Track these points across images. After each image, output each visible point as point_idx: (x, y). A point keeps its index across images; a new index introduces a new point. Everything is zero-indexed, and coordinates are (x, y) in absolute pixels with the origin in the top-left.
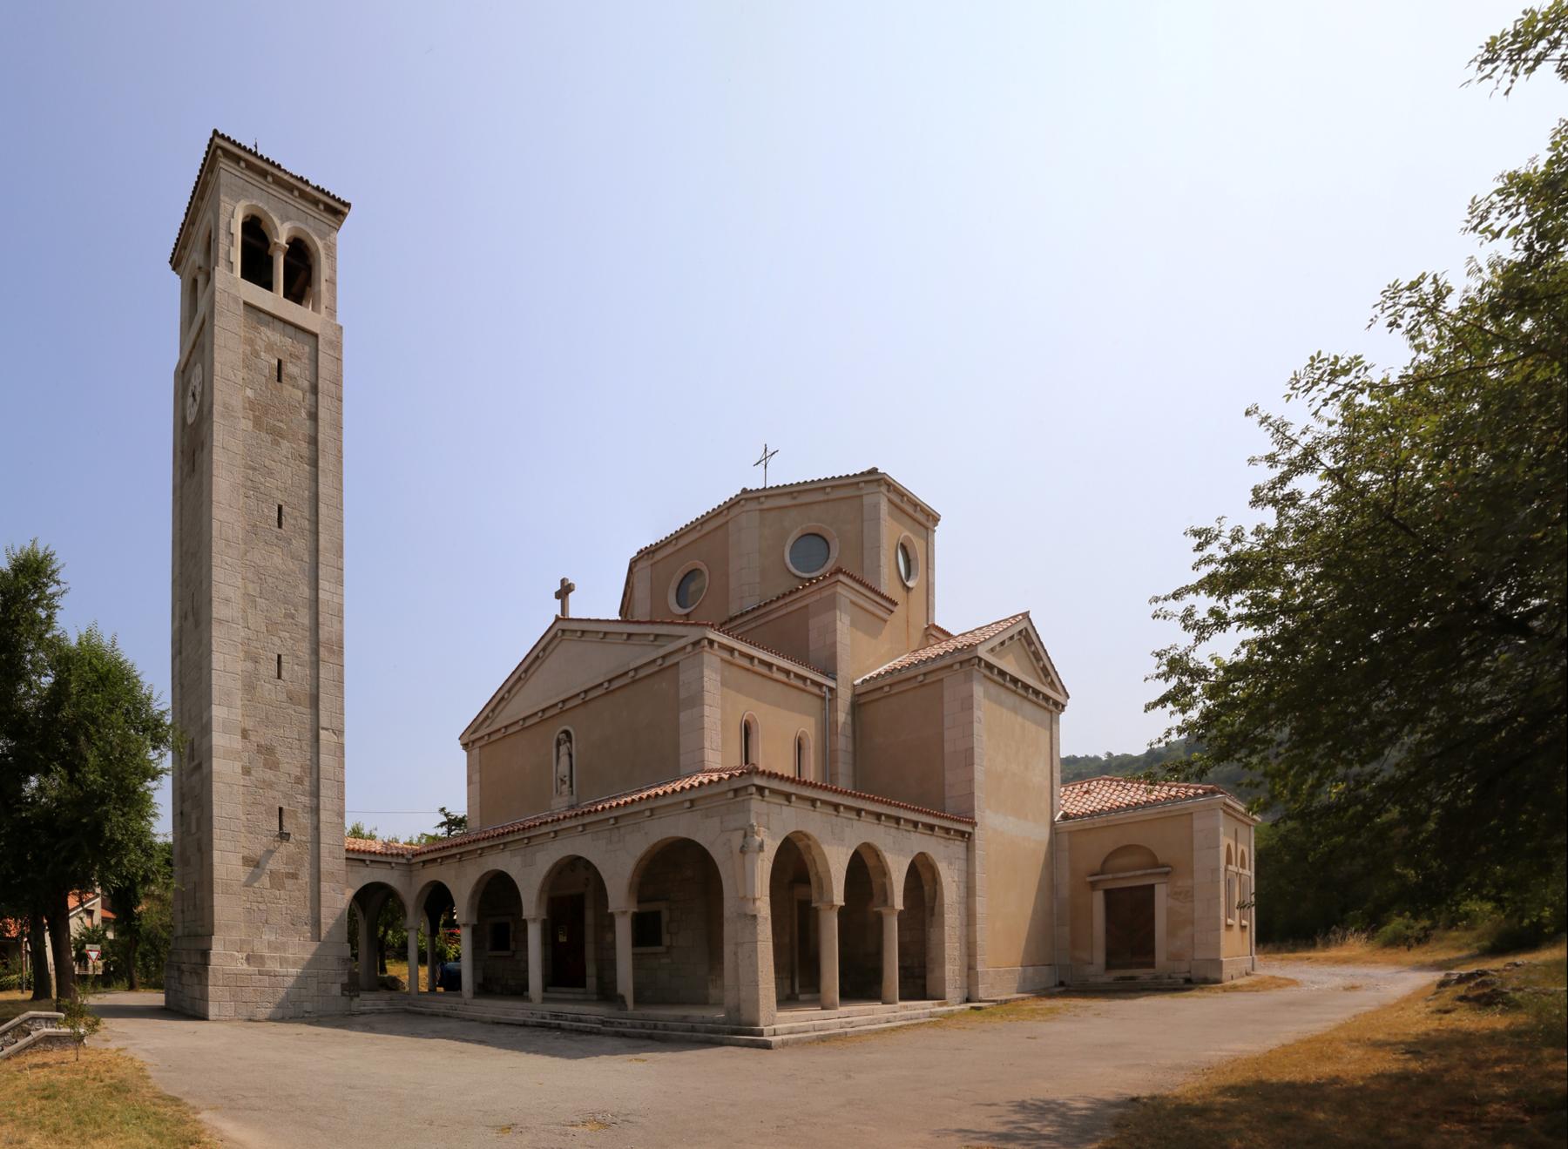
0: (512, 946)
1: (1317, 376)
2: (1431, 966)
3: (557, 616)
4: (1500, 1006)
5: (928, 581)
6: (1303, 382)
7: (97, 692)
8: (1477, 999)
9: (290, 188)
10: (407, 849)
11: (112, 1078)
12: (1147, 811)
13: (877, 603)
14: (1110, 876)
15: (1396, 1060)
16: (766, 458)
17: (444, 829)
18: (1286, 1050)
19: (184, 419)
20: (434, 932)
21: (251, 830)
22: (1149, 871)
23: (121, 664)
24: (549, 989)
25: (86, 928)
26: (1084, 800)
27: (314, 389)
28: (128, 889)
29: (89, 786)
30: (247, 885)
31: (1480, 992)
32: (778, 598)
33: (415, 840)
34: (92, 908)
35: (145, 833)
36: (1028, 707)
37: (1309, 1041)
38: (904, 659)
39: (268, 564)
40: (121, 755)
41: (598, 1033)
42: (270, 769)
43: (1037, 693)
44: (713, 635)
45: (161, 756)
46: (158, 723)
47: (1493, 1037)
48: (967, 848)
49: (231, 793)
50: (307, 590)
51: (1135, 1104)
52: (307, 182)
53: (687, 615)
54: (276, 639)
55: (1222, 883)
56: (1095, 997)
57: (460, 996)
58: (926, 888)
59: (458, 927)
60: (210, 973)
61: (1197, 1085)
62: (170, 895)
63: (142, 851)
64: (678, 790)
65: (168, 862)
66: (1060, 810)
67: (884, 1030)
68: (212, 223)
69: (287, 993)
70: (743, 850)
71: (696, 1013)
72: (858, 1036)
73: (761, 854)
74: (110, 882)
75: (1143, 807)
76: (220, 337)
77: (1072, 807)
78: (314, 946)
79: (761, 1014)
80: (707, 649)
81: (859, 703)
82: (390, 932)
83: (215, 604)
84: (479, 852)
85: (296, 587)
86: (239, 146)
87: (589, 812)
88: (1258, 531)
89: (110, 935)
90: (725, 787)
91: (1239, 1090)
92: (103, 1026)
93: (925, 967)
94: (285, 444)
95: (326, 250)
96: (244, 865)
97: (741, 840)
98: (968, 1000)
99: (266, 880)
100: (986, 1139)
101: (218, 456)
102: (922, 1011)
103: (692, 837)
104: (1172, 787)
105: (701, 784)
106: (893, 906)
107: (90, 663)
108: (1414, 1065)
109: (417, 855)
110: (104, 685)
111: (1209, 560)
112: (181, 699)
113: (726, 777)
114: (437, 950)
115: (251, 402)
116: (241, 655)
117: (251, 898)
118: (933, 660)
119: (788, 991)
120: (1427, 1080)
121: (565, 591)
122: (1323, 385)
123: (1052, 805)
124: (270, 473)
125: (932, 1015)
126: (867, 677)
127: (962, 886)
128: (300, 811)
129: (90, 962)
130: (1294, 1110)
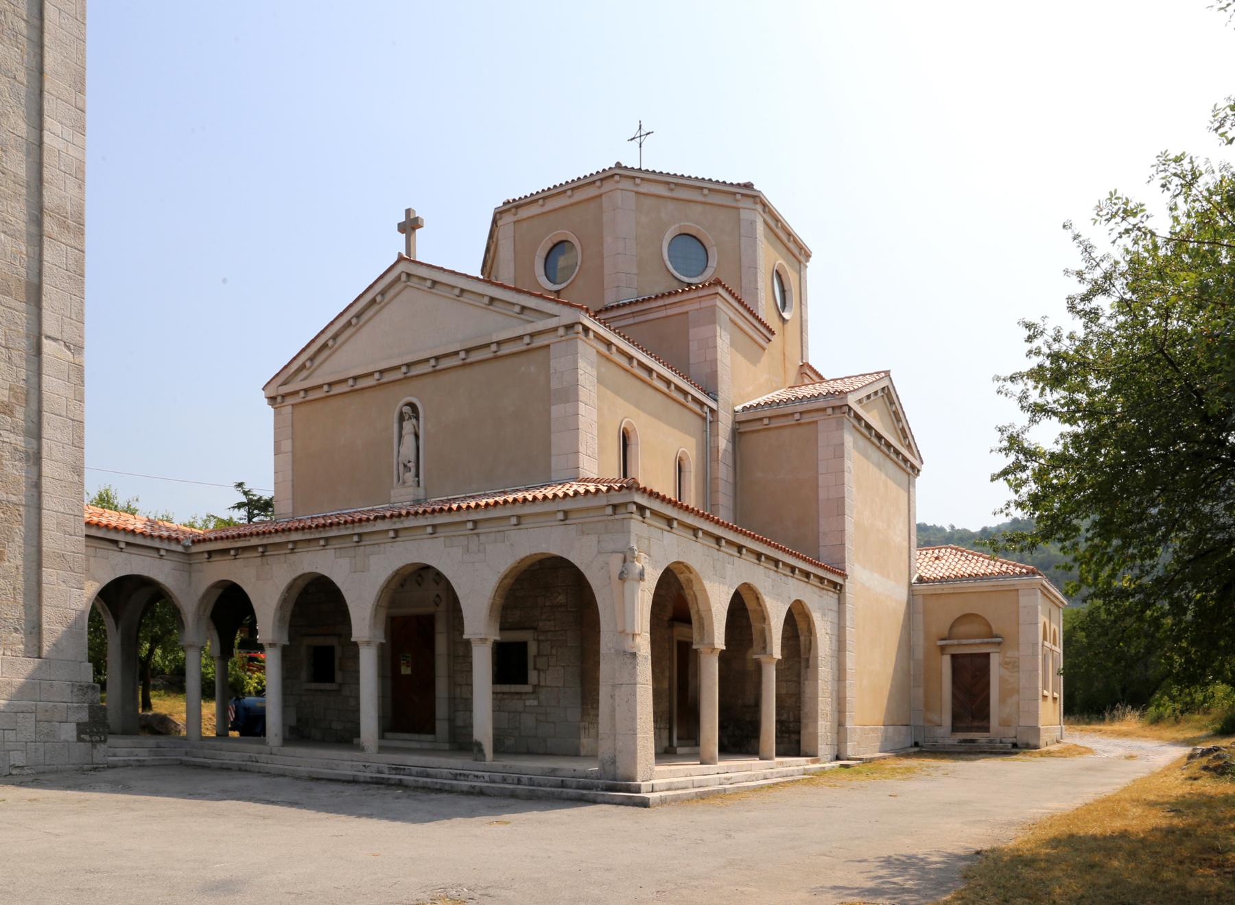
0: (339, 676)
1: (1114, 210)
2: (1182, 742)
3: (399, 253)
4: (1230, 775)
5: (801, 317)
6: (1104, 212)
8: (1215, 769)
10: (184, 532)
12: (985, 583)
13: (755, 327)
14: (955, 642)
15: (1165, 817)
16: (640, 136)
17: (243, 512)
18: (1089, 809)
20: (226, 652)
22: (986, 640)
24: (389, 735)
26: (935, 566)
31: (1217, 763)
32: (657, 297)
33: (199, 523)
36: (890, 465)
37: (1104, 801)
38: (781, 394)
41: (451, 791)
43: (897, 453)
44: (589, 322)
47: (1227, 801)
48: (839, 599)
51: (979, 857)
53: (558, 292)
55: (1040, 657)
56: (943, 758)
57: (264, 743)
58: (802, 638)
61: (1026, 839)
64: (550, 497)
66: (916, 572)
67: (762, 787)
70: (622, 577)
71: (566, 766)
72: (737, 793)
73: (641, 583)
75: (982, 579)
77: (926, 571)
78: (31, 665)
79: (639, 768)
80: (582, 336)
81: (738, 433)
82: (158, 651)
84: (290, 546)
87: (441, 510)
88: (1071, 337)
90: (602, 501)
91: (1056, 842)
93: (800, 722)
97: (621, 564)
98: (838, 758)
100: (857, 895)
102: (796, 768)
103: (565, 556)
104: (1003, 563)
105: (576, 493)
106: (772, 655)
108: (1176, 821)
109: (199, 541)
111: (1038, 353)
113: (604, 489)
118: (809, 399)
119: (666, 743)
120: (1187, 833)
121: (410, 225)
122: (1118, 219)
123: (910, 566)
125: (805, 772)
126: (747, 404)
127: (834, 638)
128: (7, 455)
130: (1097, 859)
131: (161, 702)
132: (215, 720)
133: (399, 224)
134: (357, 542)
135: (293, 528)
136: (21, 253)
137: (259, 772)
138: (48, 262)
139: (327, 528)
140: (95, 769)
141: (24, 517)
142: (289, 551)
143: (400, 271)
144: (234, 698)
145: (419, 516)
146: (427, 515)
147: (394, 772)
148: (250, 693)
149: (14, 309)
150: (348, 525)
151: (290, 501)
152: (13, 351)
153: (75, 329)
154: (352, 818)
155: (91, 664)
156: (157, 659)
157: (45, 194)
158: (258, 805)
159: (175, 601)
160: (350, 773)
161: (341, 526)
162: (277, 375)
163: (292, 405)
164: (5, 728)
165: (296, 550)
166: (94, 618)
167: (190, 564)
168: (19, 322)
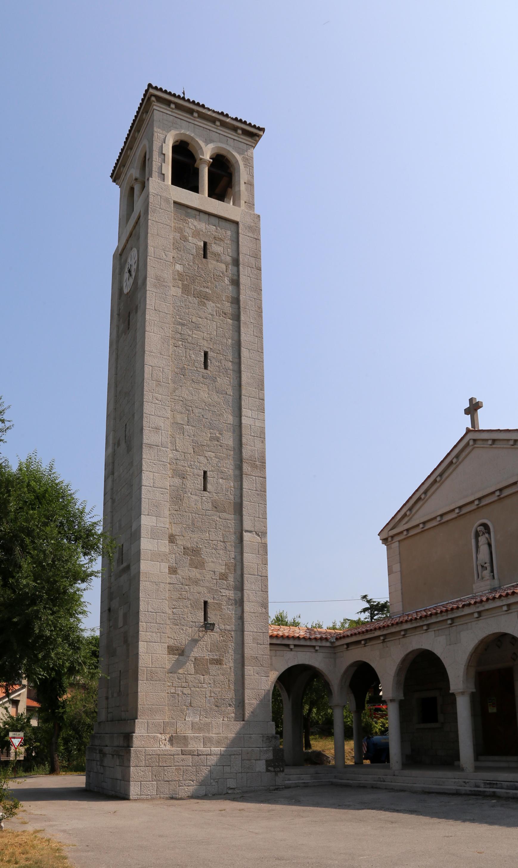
0: (441, 718)
3: (467, 428)
7: (33, 509)
9: (213, 120)
10: (330, 633)
11: (27, 859)
17: (367, 614)
19: (121, 290)
20: (360, 707)
21: (177, 621)
23: (57, 484)
25: (11, 717)
27: (236, 262)
28: (54, 680)
29: (21, 589)
30: (172, 671)
33: (338, 625)
34: (18, 698)
35: (73, 629)
39: (195, 398)
40: (53, 561)
42: (196, 568)
45: (91, 561)
46: (89, 533)
49: (158, 590)
50: (231, 417)
52: (227, 115)
54: (202, 459)
57: (389, 768)
59: (384, 702)
60: (133, 755)
62: (95, 684)
63: (70, 645)
65: (94, 654)
68: (147, 146)
69: (210, 772)
74: (37, 674)
76: (153, 228)
78: (238, 726)
82: (315, 710)
83: (146, 432)
85: (221, 415)
86: (170, 93)
89: (34, 723)
92: (21, 809)
94: (210, 305)
95: (243, 161)
96: (169, 653)
99: (190, 667)
101: (150, 316)
107: (28, 485)
109: (340, 638)
110: (40, 503)
112: (112, 512)
114: (363, 724)
115: (179, 274)
116: (170, 473)
117: (175, 684)
124: (197, 327)
128: (224, 603)
129: (13, 749)
131: (317, 743)
132: (353, 753)
133: (113, 182)
134: (451, 624)
135: (404, 621)
136: (231, 487)
137: (386, 789)
138: (246, 489)
139: (428, 618)
140: (277, 789)
141: (234, 638)
142: (402, 637)
143: (469, 439)
144: (366, 737)
145: (496, 600)
146: (503, 598)
147: (488, 786)
148: (376, 732)
149: (227, 519)
150: (443, 614)
151: (401, 603)
152: (227, 543)
153: (262, 523)
154: (459, 822)
155: (274, 723)
156: (314, 715)
157: (243, 451)
158: (387, 812)
159: (331, 687)
160: (454, 787)
161: (438, 615)
162: (388, 524)
163: (399, 541)
164: (224, 765)
165: (406, 636)
166: (276, 694)
167: (335, 653)
168: (230, 526)
